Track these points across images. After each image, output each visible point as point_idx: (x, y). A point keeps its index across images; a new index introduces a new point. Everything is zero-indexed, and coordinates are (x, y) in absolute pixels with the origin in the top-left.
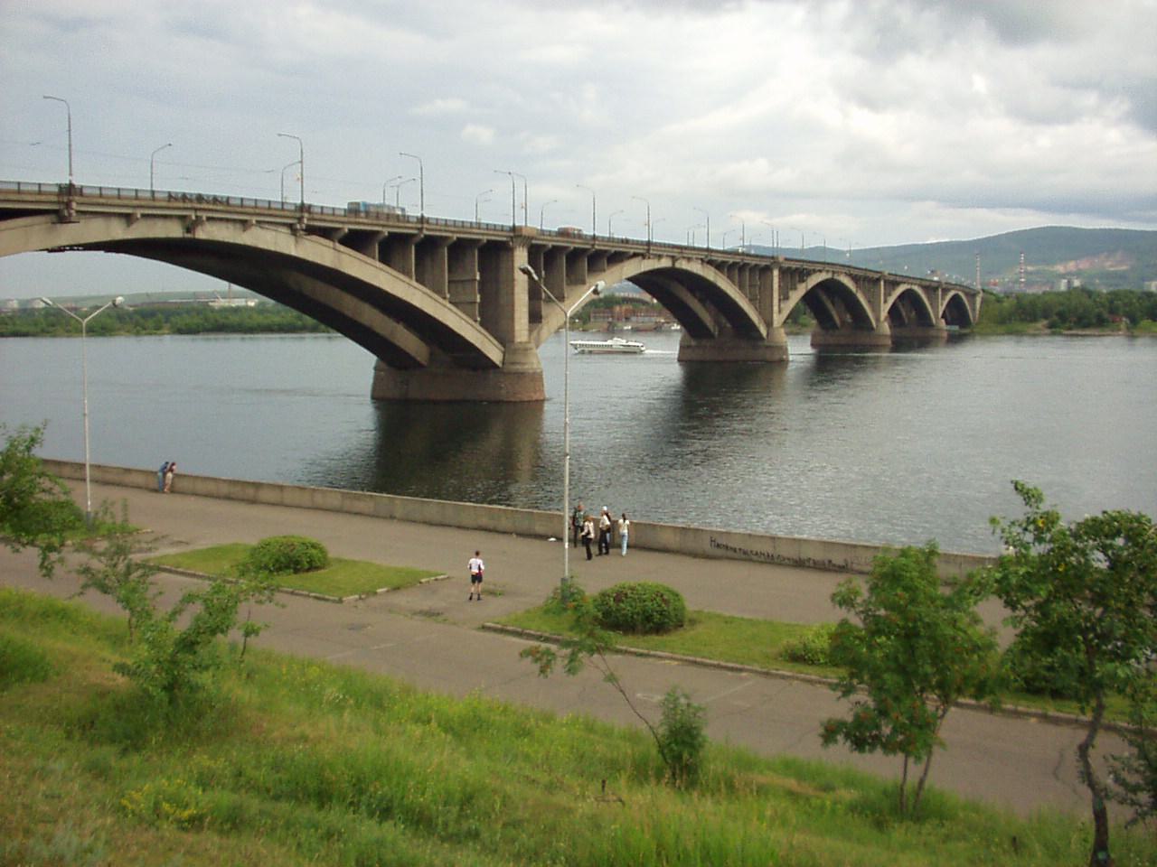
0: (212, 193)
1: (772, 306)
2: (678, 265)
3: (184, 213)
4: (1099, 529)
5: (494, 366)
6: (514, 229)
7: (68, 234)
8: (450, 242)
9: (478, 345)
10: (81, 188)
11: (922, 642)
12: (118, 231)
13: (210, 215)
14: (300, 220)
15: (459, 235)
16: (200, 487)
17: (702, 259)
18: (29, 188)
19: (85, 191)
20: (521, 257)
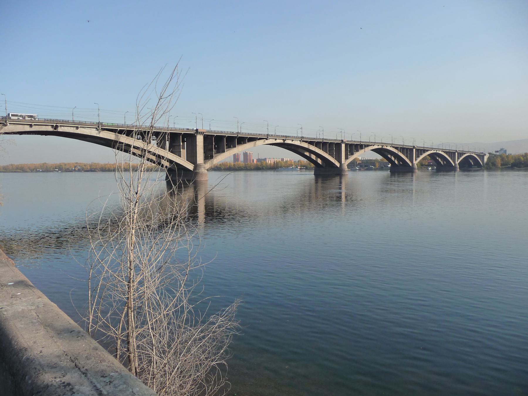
0: (285, 135)
5: (410, 166)
11: (41, 360)
14: (301, 140)
20: (343, 146)
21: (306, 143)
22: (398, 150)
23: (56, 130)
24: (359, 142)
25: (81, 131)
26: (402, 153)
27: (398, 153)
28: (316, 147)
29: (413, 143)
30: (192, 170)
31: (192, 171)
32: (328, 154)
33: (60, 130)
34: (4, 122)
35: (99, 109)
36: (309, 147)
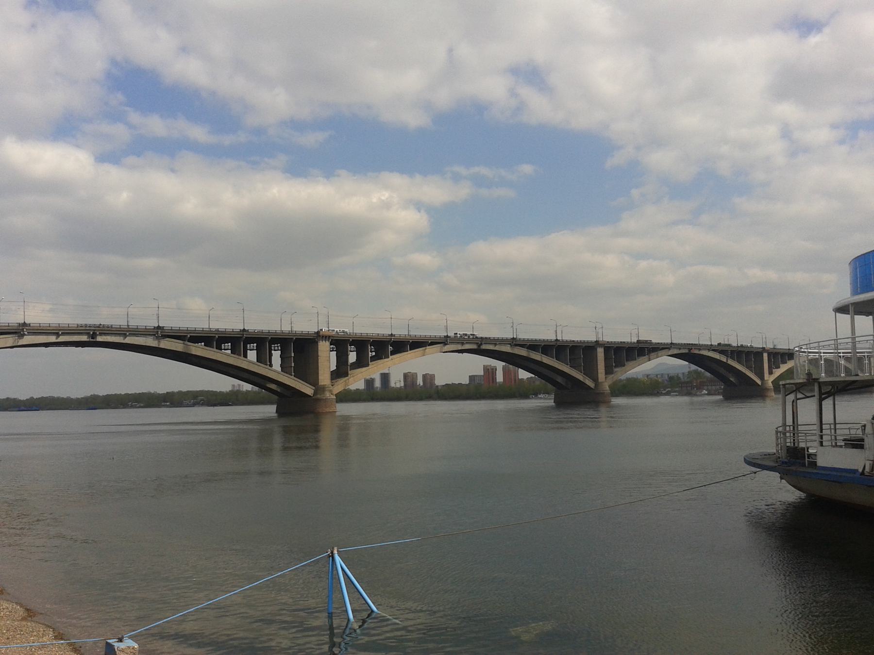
2: (692, 351)
3: (88, 332)
4: (329, 648)
5: (759, 385)
7: (447, 348)
8: (569, 347)
10: (395, 335)
12: (460, 347)
13: (100, 332)
14: (513, 342)
15: (297, 337)
16: (795, 408)
17: (708, 349)
18: (311, 333)
19: (249, 331)
20: (765, 355)
22: (728, 357)
23: (94, 339)
24: (786, 349)
25: (129, 340)
26: (738, 362)
27: (727, 360)
28: (543, 355)
29: (597, 333)
30: (312, 395)
31: (310, 396)
32: (568, 366)
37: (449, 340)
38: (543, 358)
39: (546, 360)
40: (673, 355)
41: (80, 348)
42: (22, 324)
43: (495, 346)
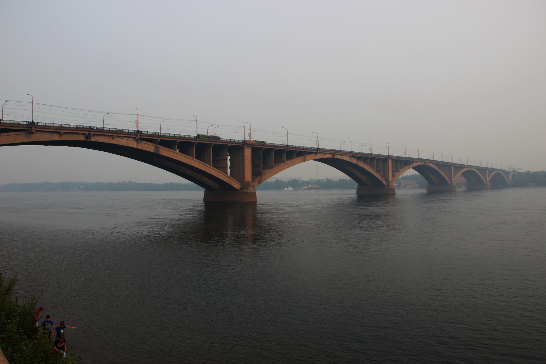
1: (388, 174)
2: (335, 157)
5: (385, 186)
6: (388, 156)
7: (33, 138)
8: (364, 157)
9: (227, 182)
14: (351, 154)
15: (310, 151)
20: (390, 161)
21: (355, 159)
30: (239, 190)
32: (375, 171)
33: (93, 139)
34: (30, 129)
35: (138, 115)
36: (358, 162)
37: (199, 140)
38: (364, 166)
39: (361, 164)
40: (316, 159)
41: (44, 146)
42: (31, 123)
43: (325, 155)
